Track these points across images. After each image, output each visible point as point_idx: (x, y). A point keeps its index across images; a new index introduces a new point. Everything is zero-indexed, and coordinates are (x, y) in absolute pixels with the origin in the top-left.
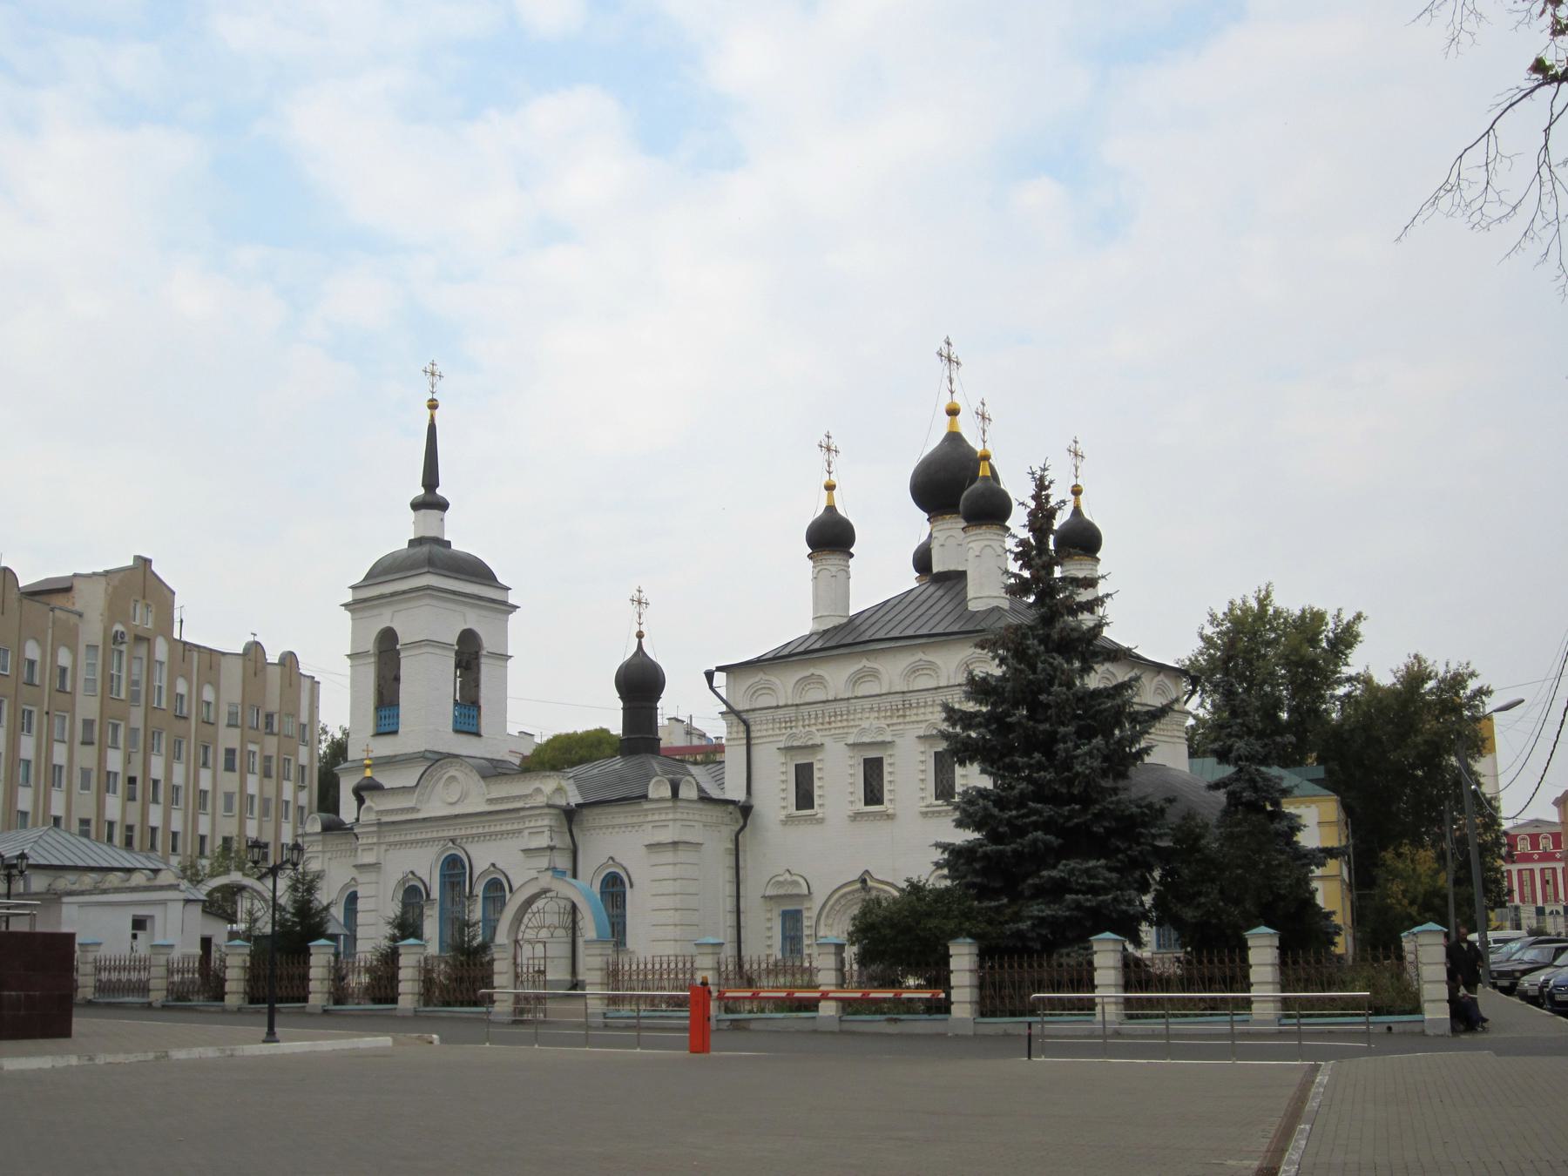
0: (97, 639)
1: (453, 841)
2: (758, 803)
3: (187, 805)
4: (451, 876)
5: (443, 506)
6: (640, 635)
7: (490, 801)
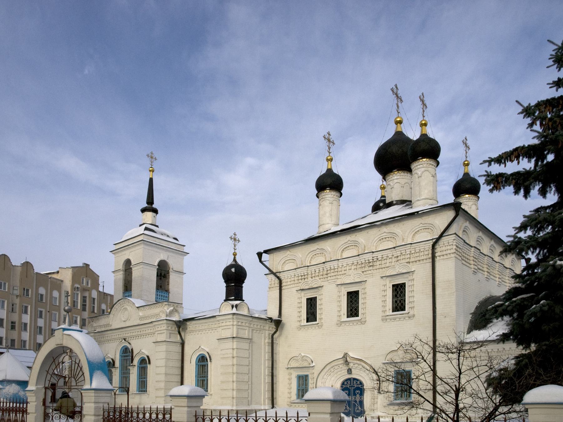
0: (69, 289)
1: (125, 339)
2: (284, 319)
3: (45, 333)
4: (124, 356)
5: (155, 211)
6: (235, 255)
7: (141, 318)
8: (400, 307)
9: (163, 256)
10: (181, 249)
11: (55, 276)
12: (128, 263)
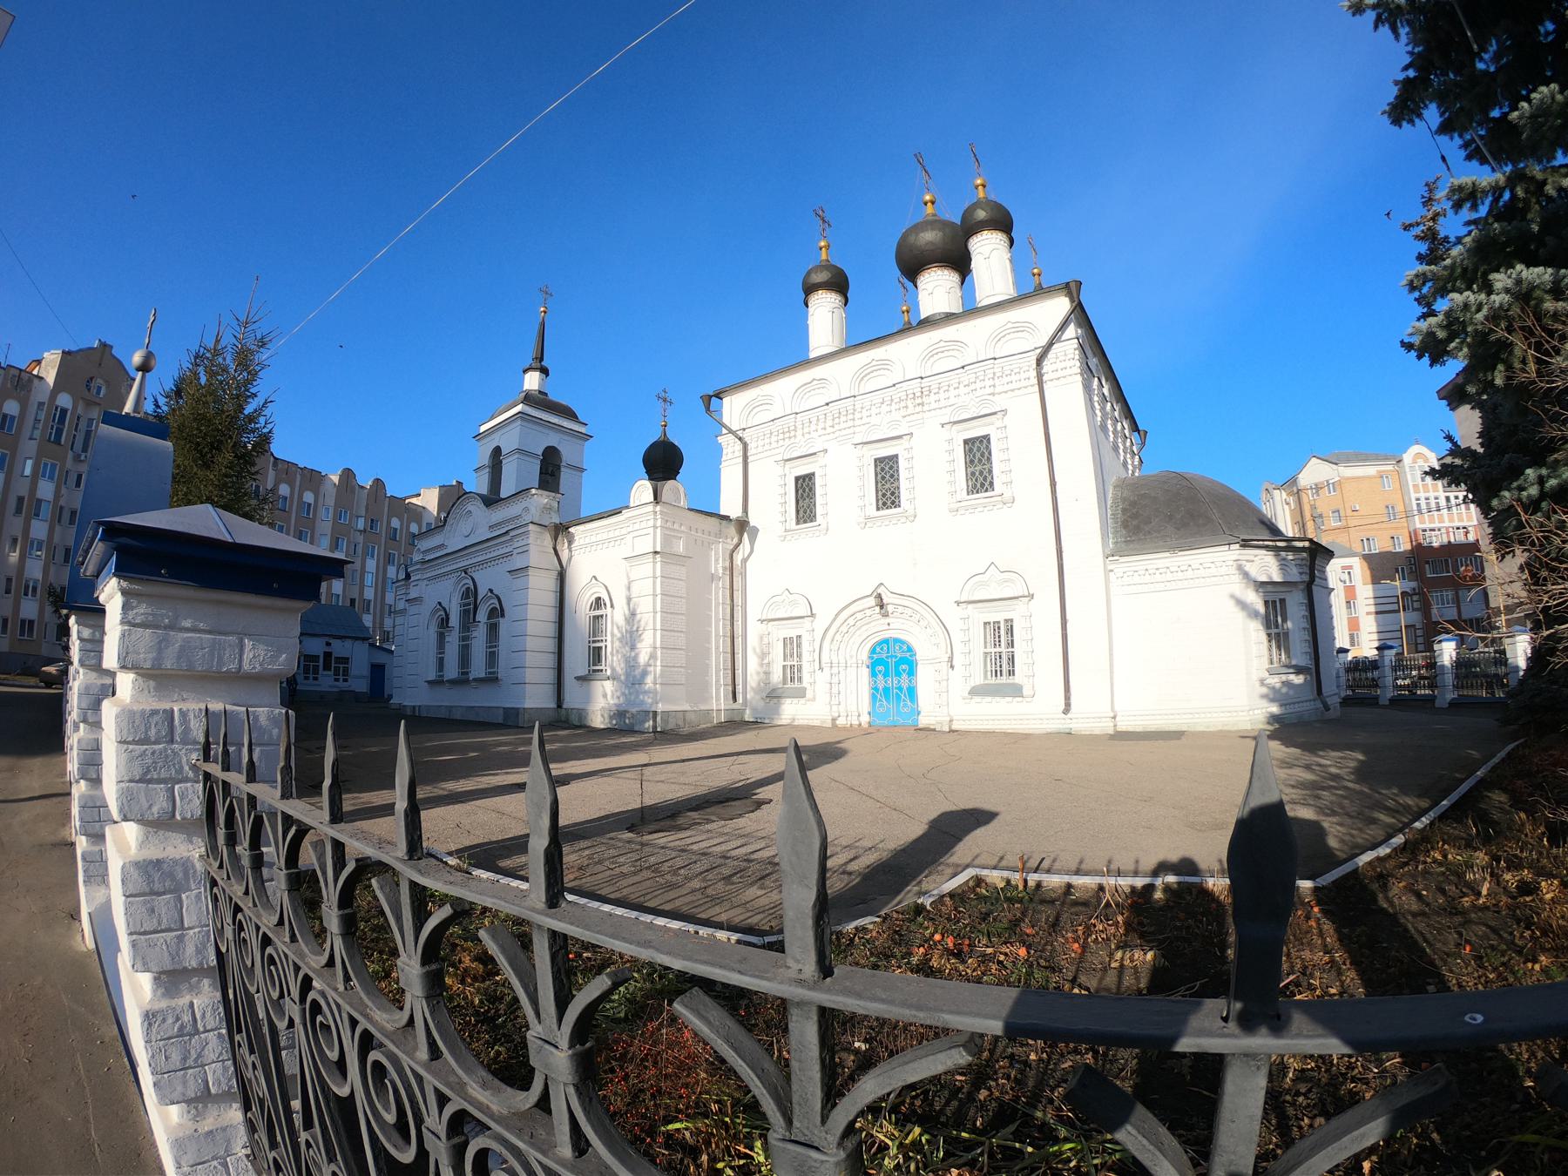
8: (982, 485)
9: (553, 440)
10: (583, 430)
11: (414, 501)
12: (497, 451)
